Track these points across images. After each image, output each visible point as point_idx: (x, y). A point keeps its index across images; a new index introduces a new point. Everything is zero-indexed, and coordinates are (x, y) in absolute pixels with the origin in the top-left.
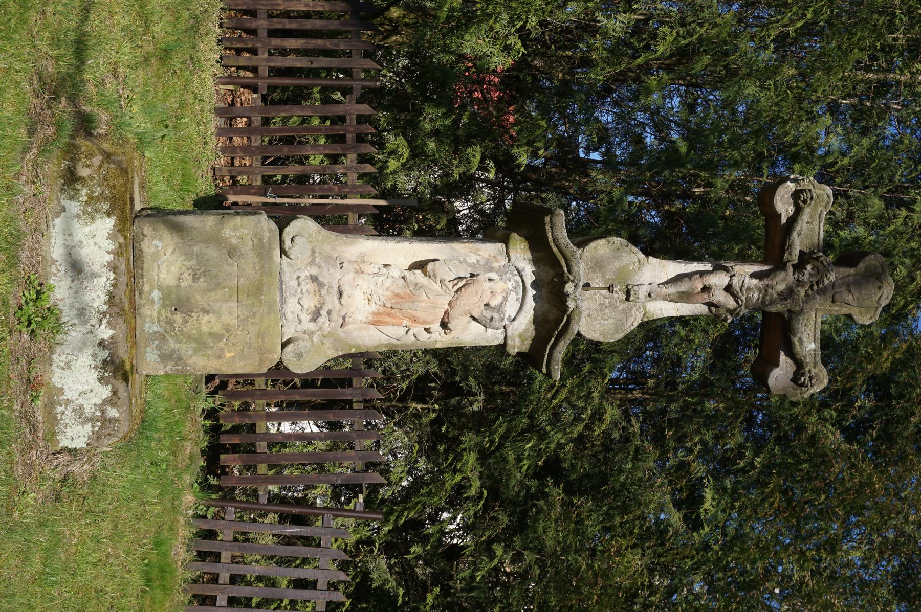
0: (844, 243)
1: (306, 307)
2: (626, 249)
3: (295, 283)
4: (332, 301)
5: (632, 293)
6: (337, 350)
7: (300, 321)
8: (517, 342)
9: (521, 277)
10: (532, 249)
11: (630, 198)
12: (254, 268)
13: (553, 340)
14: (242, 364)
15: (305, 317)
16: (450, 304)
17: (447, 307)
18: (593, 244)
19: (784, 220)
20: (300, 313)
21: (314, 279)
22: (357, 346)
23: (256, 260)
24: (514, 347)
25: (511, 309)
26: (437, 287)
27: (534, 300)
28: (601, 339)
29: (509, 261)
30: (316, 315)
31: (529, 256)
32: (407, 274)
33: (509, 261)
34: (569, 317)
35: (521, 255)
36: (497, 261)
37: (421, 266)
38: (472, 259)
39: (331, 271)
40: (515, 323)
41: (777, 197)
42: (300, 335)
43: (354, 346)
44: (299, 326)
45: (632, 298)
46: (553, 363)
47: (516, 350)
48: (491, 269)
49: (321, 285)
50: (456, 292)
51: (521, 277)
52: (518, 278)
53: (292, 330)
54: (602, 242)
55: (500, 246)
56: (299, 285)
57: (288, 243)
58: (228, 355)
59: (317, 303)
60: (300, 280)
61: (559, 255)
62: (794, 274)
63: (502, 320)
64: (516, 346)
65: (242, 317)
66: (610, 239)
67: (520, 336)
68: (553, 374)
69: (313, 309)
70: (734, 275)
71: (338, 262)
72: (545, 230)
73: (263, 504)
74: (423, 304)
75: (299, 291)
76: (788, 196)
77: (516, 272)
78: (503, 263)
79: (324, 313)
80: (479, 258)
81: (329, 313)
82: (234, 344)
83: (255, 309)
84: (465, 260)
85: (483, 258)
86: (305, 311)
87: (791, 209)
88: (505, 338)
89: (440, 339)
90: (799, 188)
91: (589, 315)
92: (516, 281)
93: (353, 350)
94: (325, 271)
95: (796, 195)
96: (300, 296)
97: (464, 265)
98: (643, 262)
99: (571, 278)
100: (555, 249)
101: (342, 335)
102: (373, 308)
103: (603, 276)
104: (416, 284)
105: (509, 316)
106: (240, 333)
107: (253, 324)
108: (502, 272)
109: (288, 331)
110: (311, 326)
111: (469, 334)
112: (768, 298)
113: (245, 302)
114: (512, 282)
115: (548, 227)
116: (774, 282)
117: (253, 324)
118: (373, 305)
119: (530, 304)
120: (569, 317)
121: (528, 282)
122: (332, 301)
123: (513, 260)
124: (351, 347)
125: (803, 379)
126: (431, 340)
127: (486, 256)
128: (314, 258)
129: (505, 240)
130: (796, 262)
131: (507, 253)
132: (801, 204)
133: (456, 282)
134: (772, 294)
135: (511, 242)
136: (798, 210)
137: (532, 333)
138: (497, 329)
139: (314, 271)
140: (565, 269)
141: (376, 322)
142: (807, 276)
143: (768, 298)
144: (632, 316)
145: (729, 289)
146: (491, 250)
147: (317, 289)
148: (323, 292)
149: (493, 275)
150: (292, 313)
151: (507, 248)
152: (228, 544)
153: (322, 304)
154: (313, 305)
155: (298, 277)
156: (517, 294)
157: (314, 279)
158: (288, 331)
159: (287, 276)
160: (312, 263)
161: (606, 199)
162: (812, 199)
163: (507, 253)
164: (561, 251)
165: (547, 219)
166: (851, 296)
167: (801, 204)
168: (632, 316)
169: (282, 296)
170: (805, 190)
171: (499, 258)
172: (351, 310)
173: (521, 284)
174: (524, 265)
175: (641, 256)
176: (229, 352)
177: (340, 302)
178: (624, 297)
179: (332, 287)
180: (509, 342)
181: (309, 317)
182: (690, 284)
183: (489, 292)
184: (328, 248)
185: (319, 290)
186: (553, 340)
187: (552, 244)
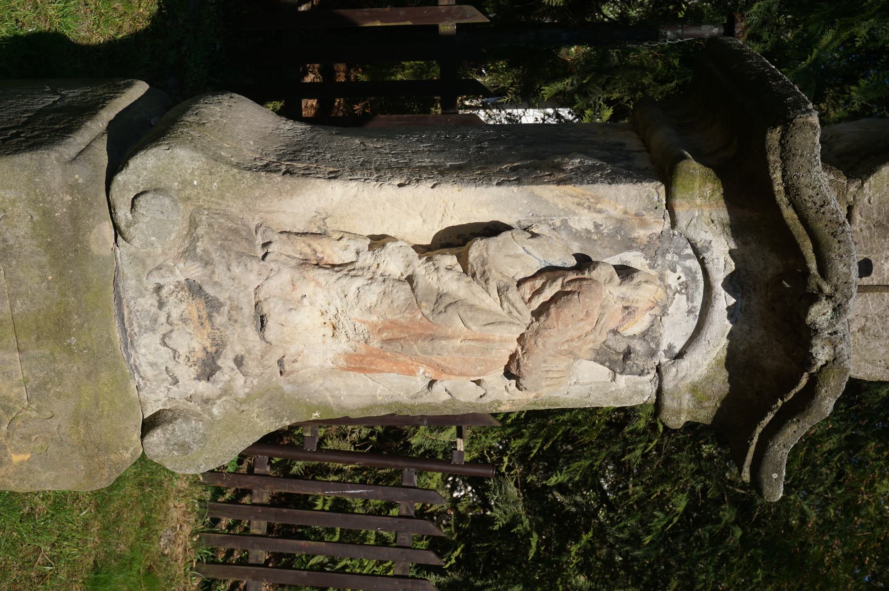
1: (183, 351)
3: (148, 302)
4: (243, 338)
6: (278, 417)
7: (176, 382)
8: (687, 401)
9: (702, 262)
10: (731, 199)
12: (43, 278)
13: (770, 417)
14: (49, 475)
15: (186, 373)
16: (521, 339)
17: (514, 346)
20: (171, 364)
21: (194, 289)
22: (324, 407)
23: (44, 260)
24: (679, 413)
25: (675, 332)
26: (490, 301)
27: (731, 316)
29: (674, 224)
30: (208, 369)
31: (723, 214)
32: (420, 267)
33: (674, 224)
34: (813, 381)
35: (703, 216)
36: (644, 224)
37: (456, 240)
38: (584, 221)
39: (237, 270)
40: (684, 363)
42: (183, 405)
43: (317, 408)
44: (174, 388)
46: (767, 466)
47: (684, 419)
48: (629, 244)
49: (213, 305)
50: (537, 314)
51: (702, 262)
52: (694, 264)
53: (162, 396)
55: (654, 190)
56: (161, 305)
57: (123, 213)
58: (16, 458)
59: (208, 343)
60: (164, 292)
61: (798, 229)
63: (653, 354)
64: (681, 411)
65: (34, 383)
67: (694, 389)
68: (767, 489)
69: (201, 355)
71: (259, 241)
72: (766, 164)
73: (311, 452)
74: (458, 343)
75: (162, 319)
77: (690, 251)
78: (658, 229)
79: (226, 362)
80: (599, 218)
81: (239, 362)
82: (26, 438)
83: (60, 366)
84: (565, 223)
85: (610, 217)
86: (182, 360)
88: (659, 392)
89: (508, 398)
91: (862, 330)
92: (688, 271)
93: (316, 415)
94: (220, 269)
96: (166, 328)
97: (564, 234)
99: (827, 289)
100: (789, 213)
101: (288, 388)
102: (343, 345)
104: (440, 296)
105: (670, 347)
106: (34, 414)
107: (58, 396)
108: (654, 250)
109: (153, 397)
110: (203, 388)
111: (576, 380)
113: (34, 352)
114: (679, 271)
115: (773, 158)
117: (58, 396)
118: (344, 339)
119: (720, 325)
120: (813, 381)
121: (719, 277)
122: (243, 338)
123: (682, 223)
124: (311, 409)
126: (487, 400)
127: (617, 213)
128: (194, 240)
129: (665, 173)
131: (670, 207)
133: (538, 283)
135: (680, 181)
137: (721, 385)
138: (641, 373)
139: (195, 271)
140: (813, 266)
141: (357, 363)
146: (628, 199)
147: (204, 313)
148: (220, 319)
149: (634, 259)
150: (152, 365)
151: (669, 195)
152: (260, 509)
153: (219, 346)
154: (198, 347)
155: (159, 288)
156: (690, 299)
157: (194, 289)
158: (153, 397)
159: (130, 285)
160: (189, 253)
163: (670, 207)
164: (804, 220)
165: (774, 137)
169: (124, 331)
171: (649, 217)
172: (292, 350)
173: (700, 276)
174: (709, 237)
176: (18, 451)
177: (263, 338)
179: (239, 309)
180: (668, 402)
181: (193, 371)
183: (620, 305)
184: (235, 207)
185: (210, 317)
186: (770, 417)
187: (782, 199)
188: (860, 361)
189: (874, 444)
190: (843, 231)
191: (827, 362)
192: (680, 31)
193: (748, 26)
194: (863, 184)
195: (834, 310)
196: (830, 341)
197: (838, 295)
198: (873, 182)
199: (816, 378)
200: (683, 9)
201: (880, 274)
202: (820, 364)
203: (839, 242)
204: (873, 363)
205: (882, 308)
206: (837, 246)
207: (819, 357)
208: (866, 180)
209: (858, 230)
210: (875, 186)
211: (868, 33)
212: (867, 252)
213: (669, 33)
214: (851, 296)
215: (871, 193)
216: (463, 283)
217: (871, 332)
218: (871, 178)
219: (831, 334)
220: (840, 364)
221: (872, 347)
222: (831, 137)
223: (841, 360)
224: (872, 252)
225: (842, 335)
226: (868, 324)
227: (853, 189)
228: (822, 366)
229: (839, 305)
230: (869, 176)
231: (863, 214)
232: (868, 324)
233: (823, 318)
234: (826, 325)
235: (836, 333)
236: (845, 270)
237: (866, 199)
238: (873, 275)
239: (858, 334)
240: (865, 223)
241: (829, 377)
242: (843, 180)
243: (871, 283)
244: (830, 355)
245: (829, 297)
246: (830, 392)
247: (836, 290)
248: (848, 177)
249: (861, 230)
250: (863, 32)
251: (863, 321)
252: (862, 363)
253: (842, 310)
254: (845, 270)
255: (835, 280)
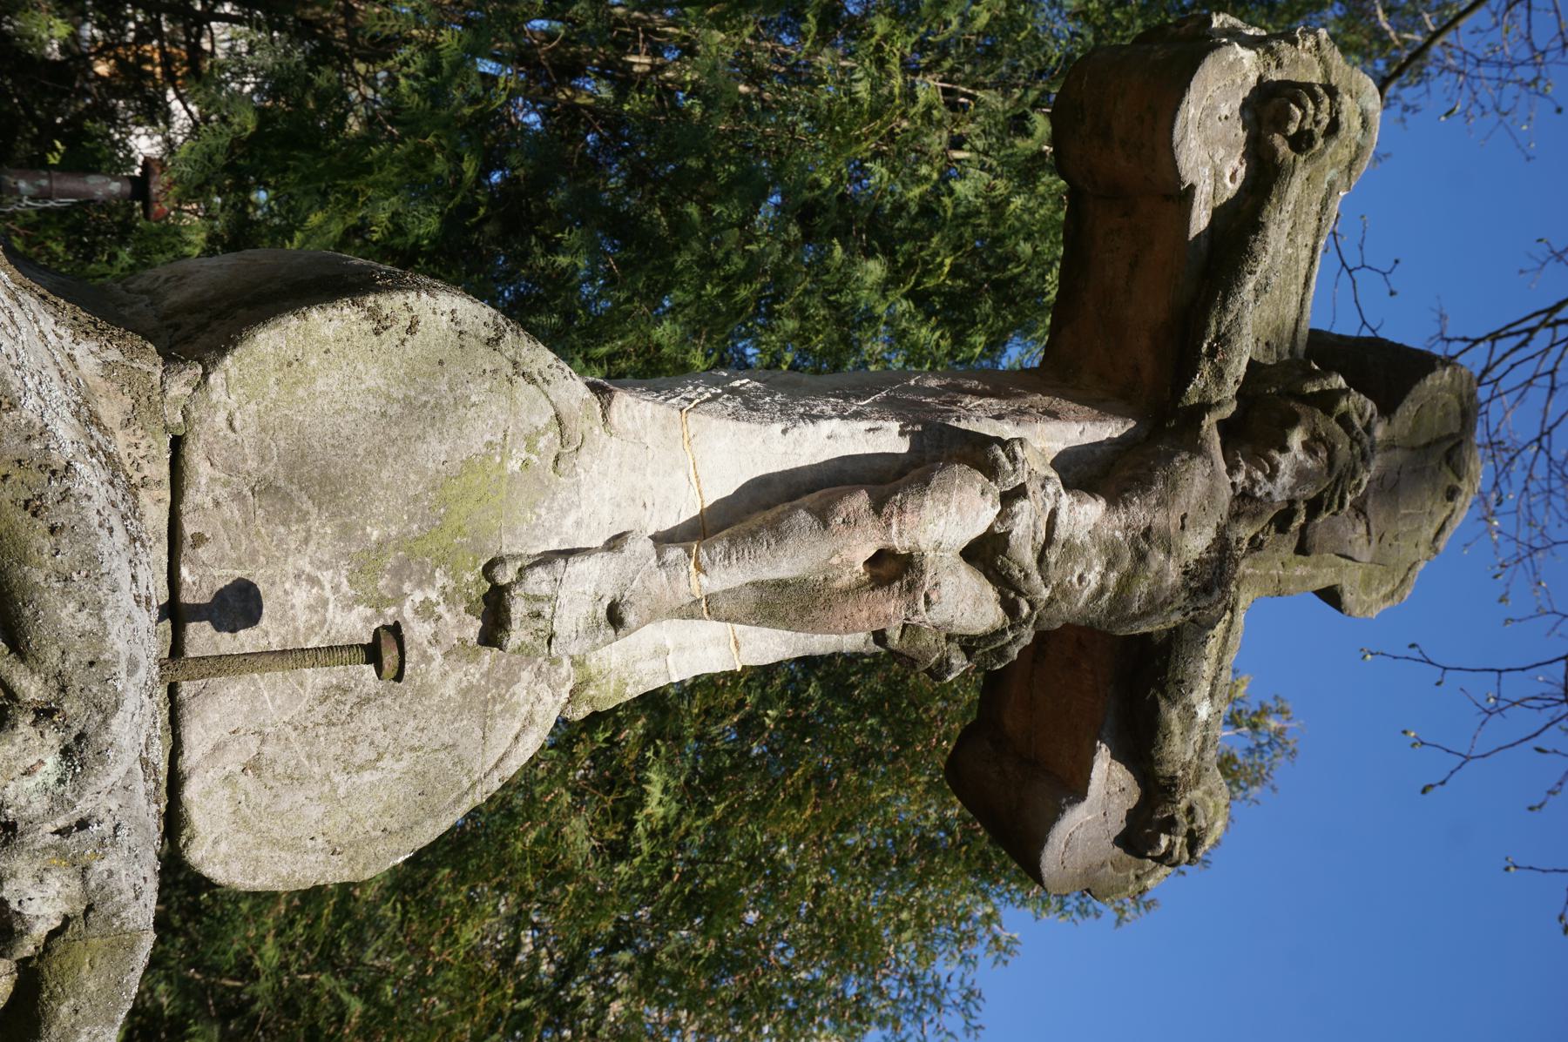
0: (961, 209)
2: (485, 359)
5: (518, 609)
11: (487, 66)
18: (271, 341)
19: (1200, 220)
28: (334, 873)
41: (1191, 109)
45: (517, 635)
54: (332, 323)
62: (1232, 469)
66: (392, 303)
70: (1020, 492)
76: (1230, 106)
87: (1233, 171)
90: (1275, 76)
91: (254, 766)
95: (1267, 107)
98: (575, 428)
99: (31, 687)
103: (345, 532)
112: (1142, 588)
116: (1175, 519)
125: (1164, 841)
130: (1228, 411)
132: (1283, 148)
134: (1161, 574)
136: (1264, 178)
142: (1285, 478)
143: (1142, 588)
144: (510, 711)
145: (985, 553)
161: (420, 61)
162: (1333, 128)
166: (1362, 529)
167: (1283, 148)
168: (510, 711)
170: (1309, 88)
175: (571, 389)
178: (474, 628)
182: (824, 549)
188: (259, 846)
189: (447, 871)
190: (65, 495)
191: (67, 920)
192: (44, 182)
193: (172, 183)
194: (206, 375)
195: (66, 752)
196: (61, 853)
197: (71, 706)
198: (233, 372)
199: (36, 972)
200: (57, 150)
201: (283, 618)
202: (41, 930)
203: (53, 530)
204: (294, 846)
205: (303, 706)
206: (47, 543)
207: (30, 910)
208: (214, 363)
209: (209, 504)
210: (242, 381)
211: (391, 219)
212: (240, 563)
213: (22, 185)
214: (117, 706)
215: (233, 402)
216: (734, 570)
217: (279, 769)
218: (228, 360)
219: (63, 832)
220: (107, 920)
221: (285, 806)
222: (167, 280)
223: (109, 907)
224: (253, 561)
225: (107, 828)
226: (267, 749)
227: (178, 388)
228: (53, 934)
229: (80, 737)
230: (222, 353)
231: (217, 460)
232: (267, 749)
233: (29, 783)
234: (40, 805)
235: (83, 824)
236: (85, 621)
237: (220, 419)
238: (264, 622)
239: (243, 779)
240: (226, 484)
241: (76, 966)
242: (150, 364)
243: (262, 645)
244: (69, 899)
245: (44, 714)
246: (87, 1010)
247: (63, 689)
248: (168, 359)
249: (217, 504)
250: (383, 217)
251: (253, 744)
252: (265, 852)
253: (89, 754)
254: (85, 621)
255: (52, 657)
